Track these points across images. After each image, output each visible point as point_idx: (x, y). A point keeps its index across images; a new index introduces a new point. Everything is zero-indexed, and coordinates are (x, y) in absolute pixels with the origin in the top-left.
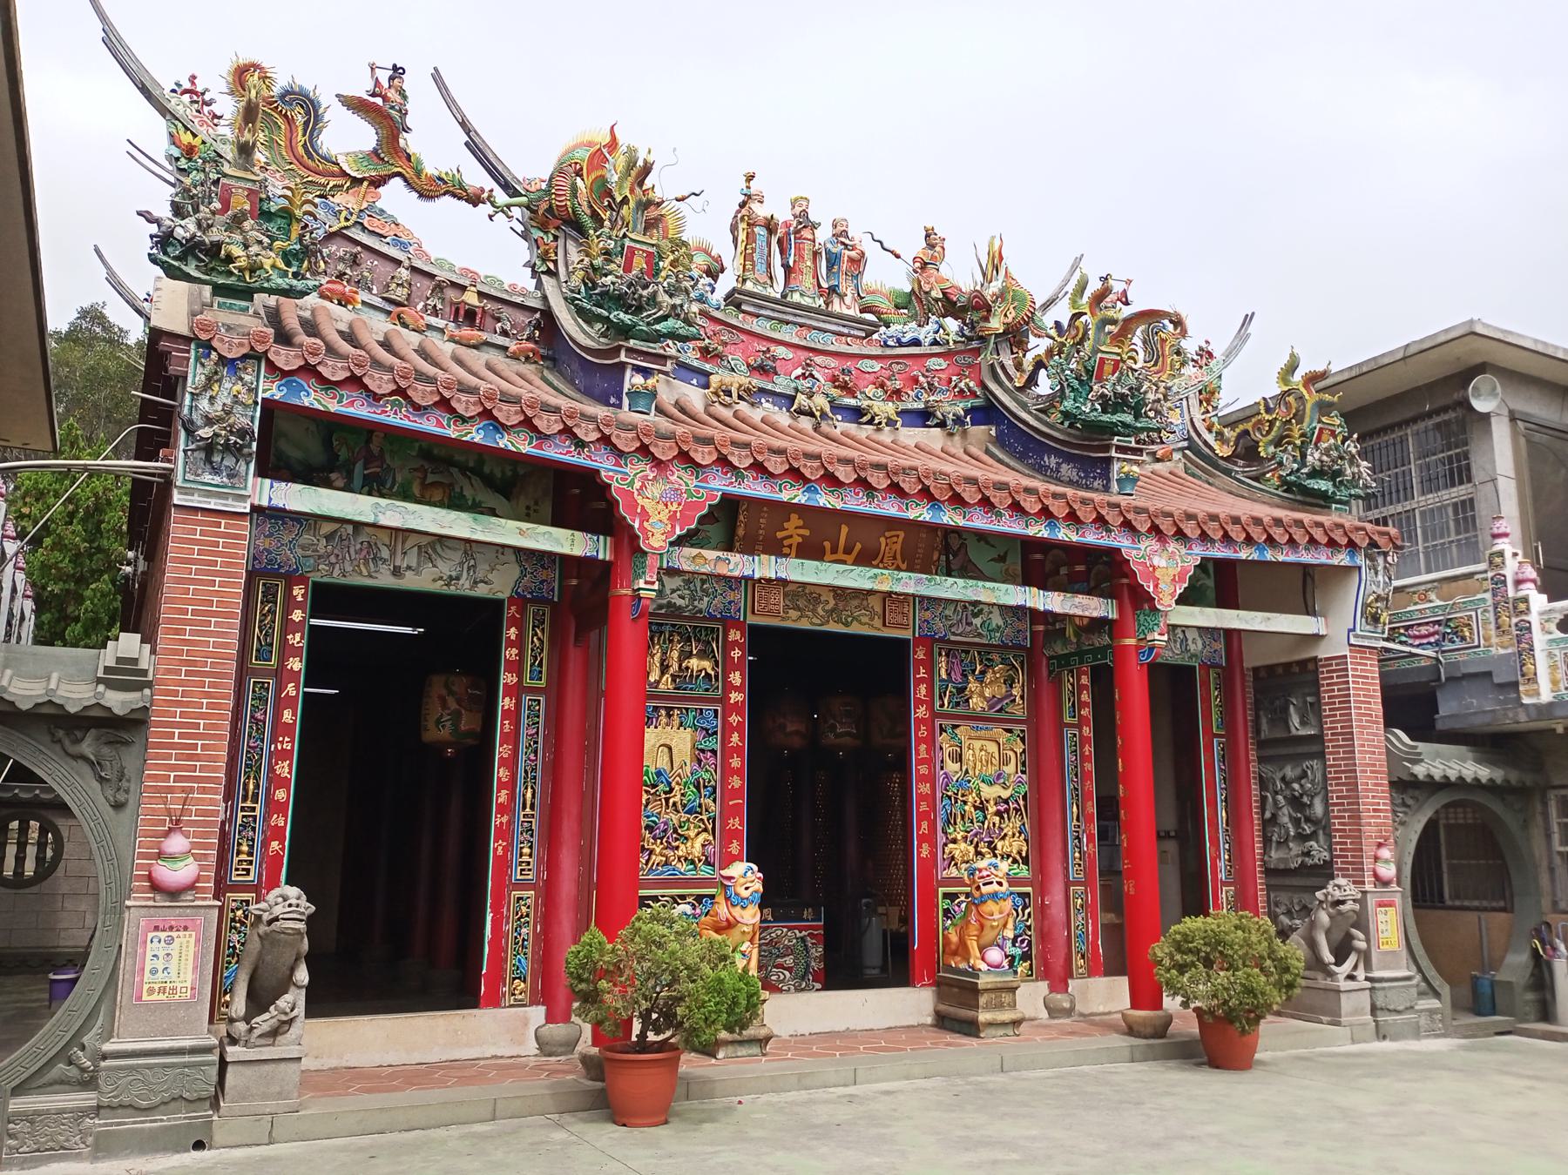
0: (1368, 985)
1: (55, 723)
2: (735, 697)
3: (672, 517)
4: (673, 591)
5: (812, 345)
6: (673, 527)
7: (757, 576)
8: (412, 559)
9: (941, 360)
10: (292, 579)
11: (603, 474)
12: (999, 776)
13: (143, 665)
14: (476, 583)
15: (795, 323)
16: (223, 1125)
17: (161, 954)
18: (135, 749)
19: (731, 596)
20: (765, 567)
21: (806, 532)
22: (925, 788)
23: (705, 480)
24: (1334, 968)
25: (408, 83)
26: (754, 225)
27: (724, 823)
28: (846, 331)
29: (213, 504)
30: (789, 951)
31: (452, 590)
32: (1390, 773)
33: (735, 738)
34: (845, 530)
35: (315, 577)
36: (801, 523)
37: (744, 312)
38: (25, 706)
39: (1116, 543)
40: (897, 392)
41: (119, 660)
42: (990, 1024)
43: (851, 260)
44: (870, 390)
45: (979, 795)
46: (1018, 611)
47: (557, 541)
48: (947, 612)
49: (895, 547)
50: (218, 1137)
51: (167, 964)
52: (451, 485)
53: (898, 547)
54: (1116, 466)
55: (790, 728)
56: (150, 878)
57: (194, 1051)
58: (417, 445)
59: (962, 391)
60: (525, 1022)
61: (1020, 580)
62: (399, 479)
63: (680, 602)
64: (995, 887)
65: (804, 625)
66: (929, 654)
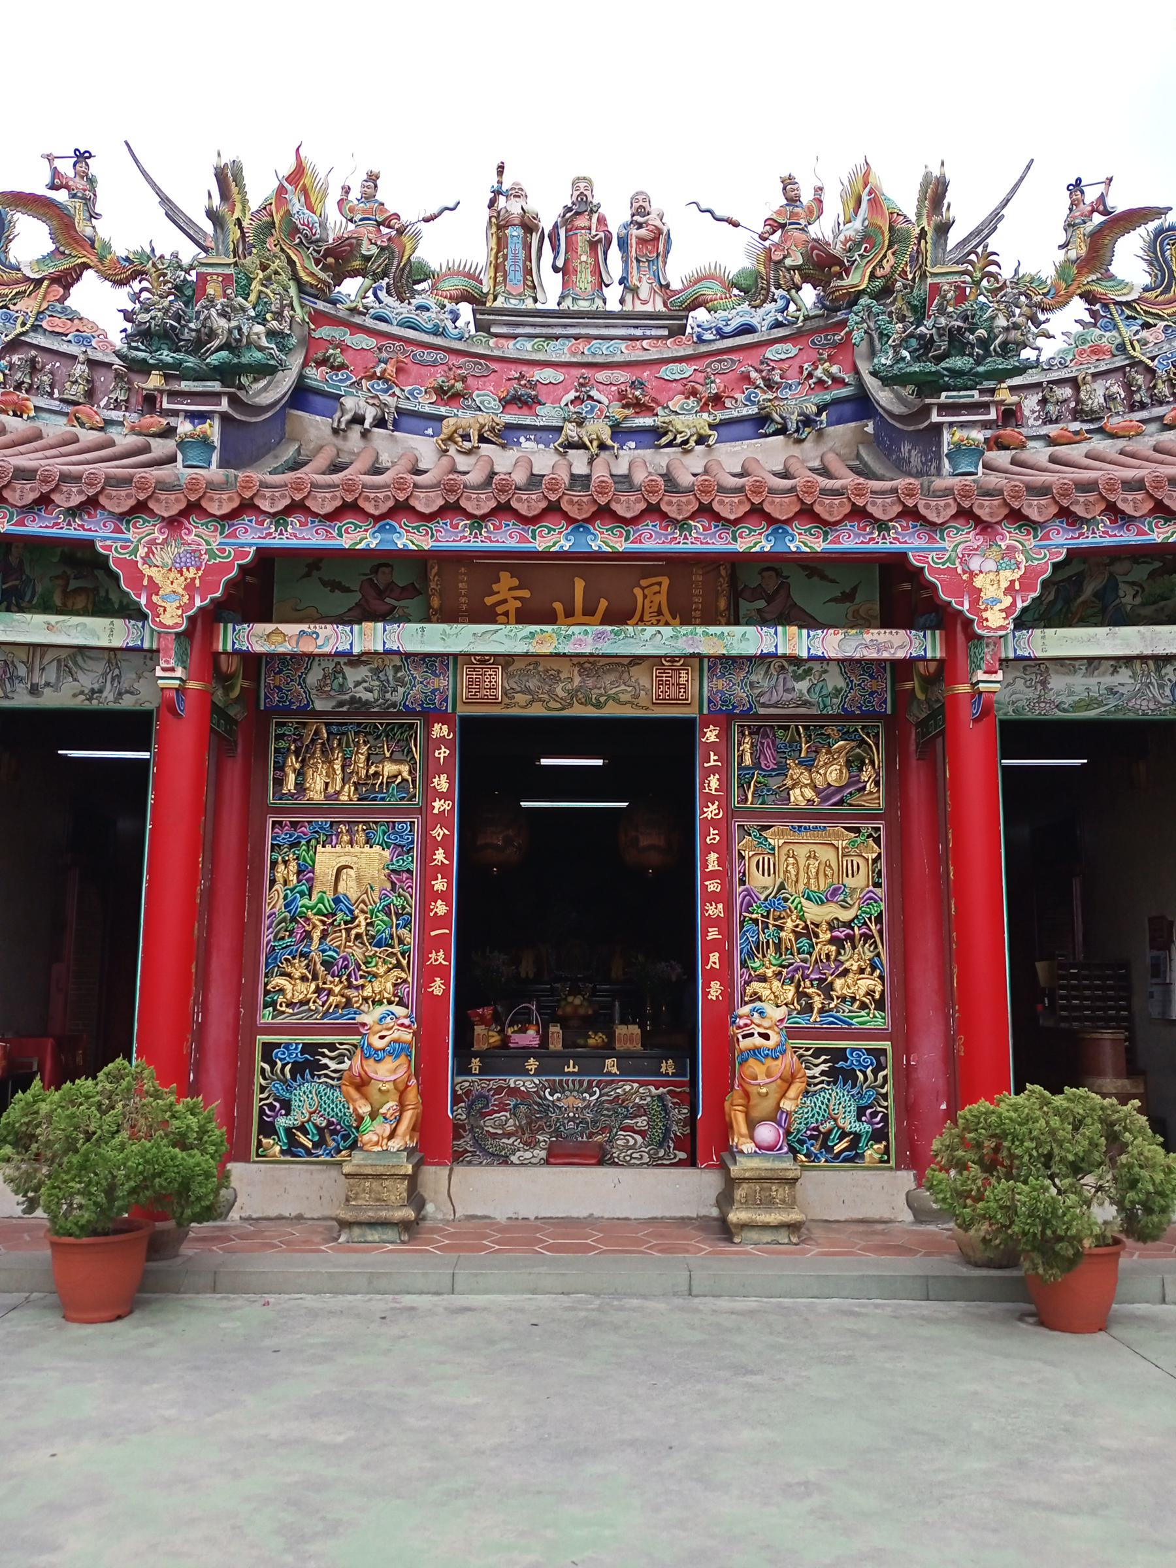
2: (438, 805)
3: (190, 587)
4: (357, 684)
5: (590, 360)
6: (192, 599)
7: (356, 651)
8: (51, 675)
9: (789, 346)
11: (98, 544)
12: (835, 892)
14: (120, 694)
15: (567, 337)
21: (526, 594)
22: (715, 910)
23: (233, 535)
25: (95, 167)
26: (506, 227)
27: (423, 957)
28: (639, 332)
30: (640, 1111)
31: (95, 704)
33: (440, 855)
34: (579, 585)
37: (496, 335)
40: (717, 400)
42: (744, 1226)
43: (642, 241)
44: (676, 403)
45: (802, 918)
46: (847, 664)
47: (93, 633)
48: (753, 678)
49: (657, 599)
52: (96, 590)
53: (663, 598)
54: (946, 437)
55: (644, 842)
58: (59, 550)
59: (820, 382)
62: (39, 589)
64: (757, 1041)
66: (725, 735)
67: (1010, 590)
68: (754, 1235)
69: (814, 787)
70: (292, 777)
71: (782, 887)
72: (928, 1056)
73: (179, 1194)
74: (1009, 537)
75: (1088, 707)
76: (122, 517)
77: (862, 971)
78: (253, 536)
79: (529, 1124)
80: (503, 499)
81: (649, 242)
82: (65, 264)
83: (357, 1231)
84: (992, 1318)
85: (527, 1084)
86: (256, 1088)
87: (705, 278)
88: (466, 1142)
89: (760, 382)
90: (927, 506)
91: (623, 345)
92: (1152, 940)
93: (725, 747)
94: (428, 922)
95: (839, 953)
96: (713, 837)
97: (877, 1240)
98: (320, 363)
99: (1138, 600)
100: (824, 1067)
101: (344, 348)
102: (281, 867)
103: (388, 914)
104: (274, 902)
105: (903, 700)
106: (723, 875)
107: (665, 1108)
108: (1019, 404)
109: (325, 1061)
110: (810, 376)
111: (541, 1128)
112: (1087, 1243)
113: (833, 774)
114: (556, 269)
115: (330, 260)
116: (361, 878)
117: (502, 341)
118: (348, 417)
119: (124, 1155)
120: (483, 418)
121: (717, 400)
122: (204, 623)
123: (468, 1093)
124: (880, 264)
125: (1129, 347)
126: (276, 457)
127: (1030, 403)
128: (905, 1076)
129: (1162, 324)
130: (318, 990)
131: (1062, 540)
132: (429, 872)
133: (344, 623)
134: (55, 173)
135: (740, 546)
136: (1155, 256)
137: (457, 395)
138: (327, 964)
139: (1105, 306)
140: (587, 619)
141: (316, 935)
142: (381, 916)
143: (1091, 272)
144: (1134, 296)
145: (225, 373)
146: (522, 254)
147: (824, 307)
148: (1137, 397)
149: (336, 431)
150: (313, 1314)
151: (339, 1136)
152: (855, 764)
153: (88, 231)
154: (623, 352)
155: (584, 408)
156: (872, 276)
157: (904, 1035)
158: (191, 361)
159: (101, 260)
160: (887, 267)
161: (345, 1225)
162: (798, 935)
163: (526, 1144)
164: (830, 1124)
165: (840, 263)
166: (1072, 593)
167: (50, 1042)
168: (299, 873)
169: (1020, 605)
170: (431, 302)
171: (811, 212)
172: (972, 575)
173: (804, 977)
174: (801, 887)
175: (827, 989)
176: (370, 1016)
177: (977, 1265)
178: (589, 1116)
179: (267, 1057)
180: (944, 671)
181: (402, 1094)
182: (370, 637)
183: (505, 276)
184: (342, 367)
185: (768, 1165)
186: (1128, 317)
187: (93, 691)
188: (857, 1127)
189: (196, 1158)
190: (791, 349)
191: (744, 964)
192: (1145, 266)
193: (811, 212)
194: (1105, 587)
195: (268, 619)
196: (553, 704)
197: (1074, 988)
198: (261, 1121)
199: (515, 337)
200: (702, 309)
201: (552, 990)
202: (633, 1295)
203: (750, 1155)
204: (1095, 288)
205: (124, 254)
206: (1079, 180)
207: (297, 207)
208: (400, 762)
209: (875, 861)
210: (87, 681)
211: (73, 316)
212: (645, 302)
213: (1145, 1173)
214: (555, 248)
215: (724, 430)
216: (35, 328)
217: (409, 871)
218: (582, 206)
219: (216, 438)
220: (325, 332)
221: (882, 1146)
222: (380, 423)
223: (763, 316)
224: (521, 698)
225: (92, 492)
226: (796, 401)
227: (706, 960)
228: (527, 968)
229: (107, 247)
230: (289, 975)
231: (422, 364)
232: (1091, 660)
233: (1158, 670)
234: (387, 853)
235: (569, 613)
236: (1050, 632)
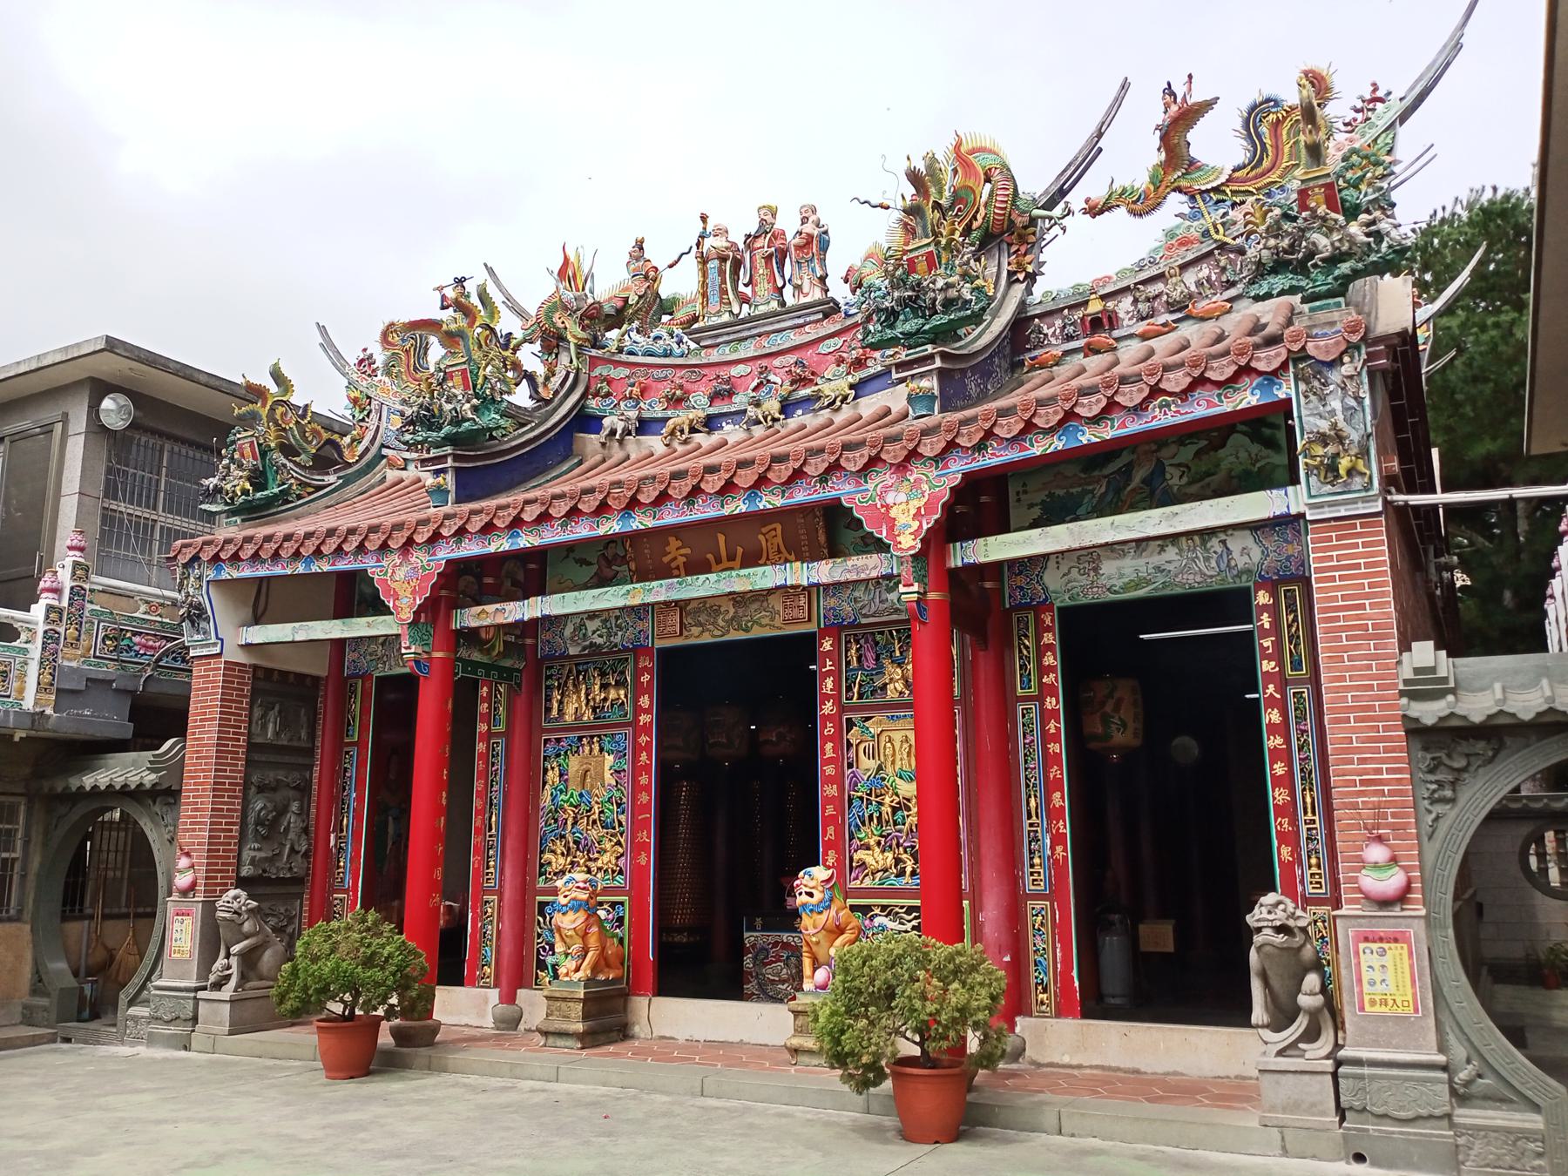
3: (414, 592)
10: (366, 677)
13: (1442, 673)
17: (1376, 966)
19: (640, 625)
20: (766, 577)
21: (687, 551)
34: (721, 538)
36: (679, 543)
38: (1527, 716)
39: (362, 566)
41: (1417, 671)
48: (856, 594)
53: (779, 540)
60: (486, 1001)
63: (599, 641)
65: (707, 639)
66: (837, 644)
67: (918, 515)
70: (555, 705)
71: (880, 768)
75: (1137, 586)
96: (829, 729)
99: (1185, 480)
100: (914, 923)
101: (609, 381)
102: (550, 773)
124: (975, 218)
125: (1212, 231)
129: (1251, 199)
134: (444, 298)
137: (679, 401)
140: (731, 564)
141: (570, 822)
143: (1175, 170)
144: (1223, 179)
154: (795, 338)
169: (925, 527)
172: (888, 507)
173: (898, 845)
181: (584, 936)
184: (608, 395)
186: (1218, 201)
194: (1152, 473)
199: (717, 345)
204: (1183, 183)
232: (1139, 541)
233: (1204, 543)
235: (719, 561)
236: (991, 539)
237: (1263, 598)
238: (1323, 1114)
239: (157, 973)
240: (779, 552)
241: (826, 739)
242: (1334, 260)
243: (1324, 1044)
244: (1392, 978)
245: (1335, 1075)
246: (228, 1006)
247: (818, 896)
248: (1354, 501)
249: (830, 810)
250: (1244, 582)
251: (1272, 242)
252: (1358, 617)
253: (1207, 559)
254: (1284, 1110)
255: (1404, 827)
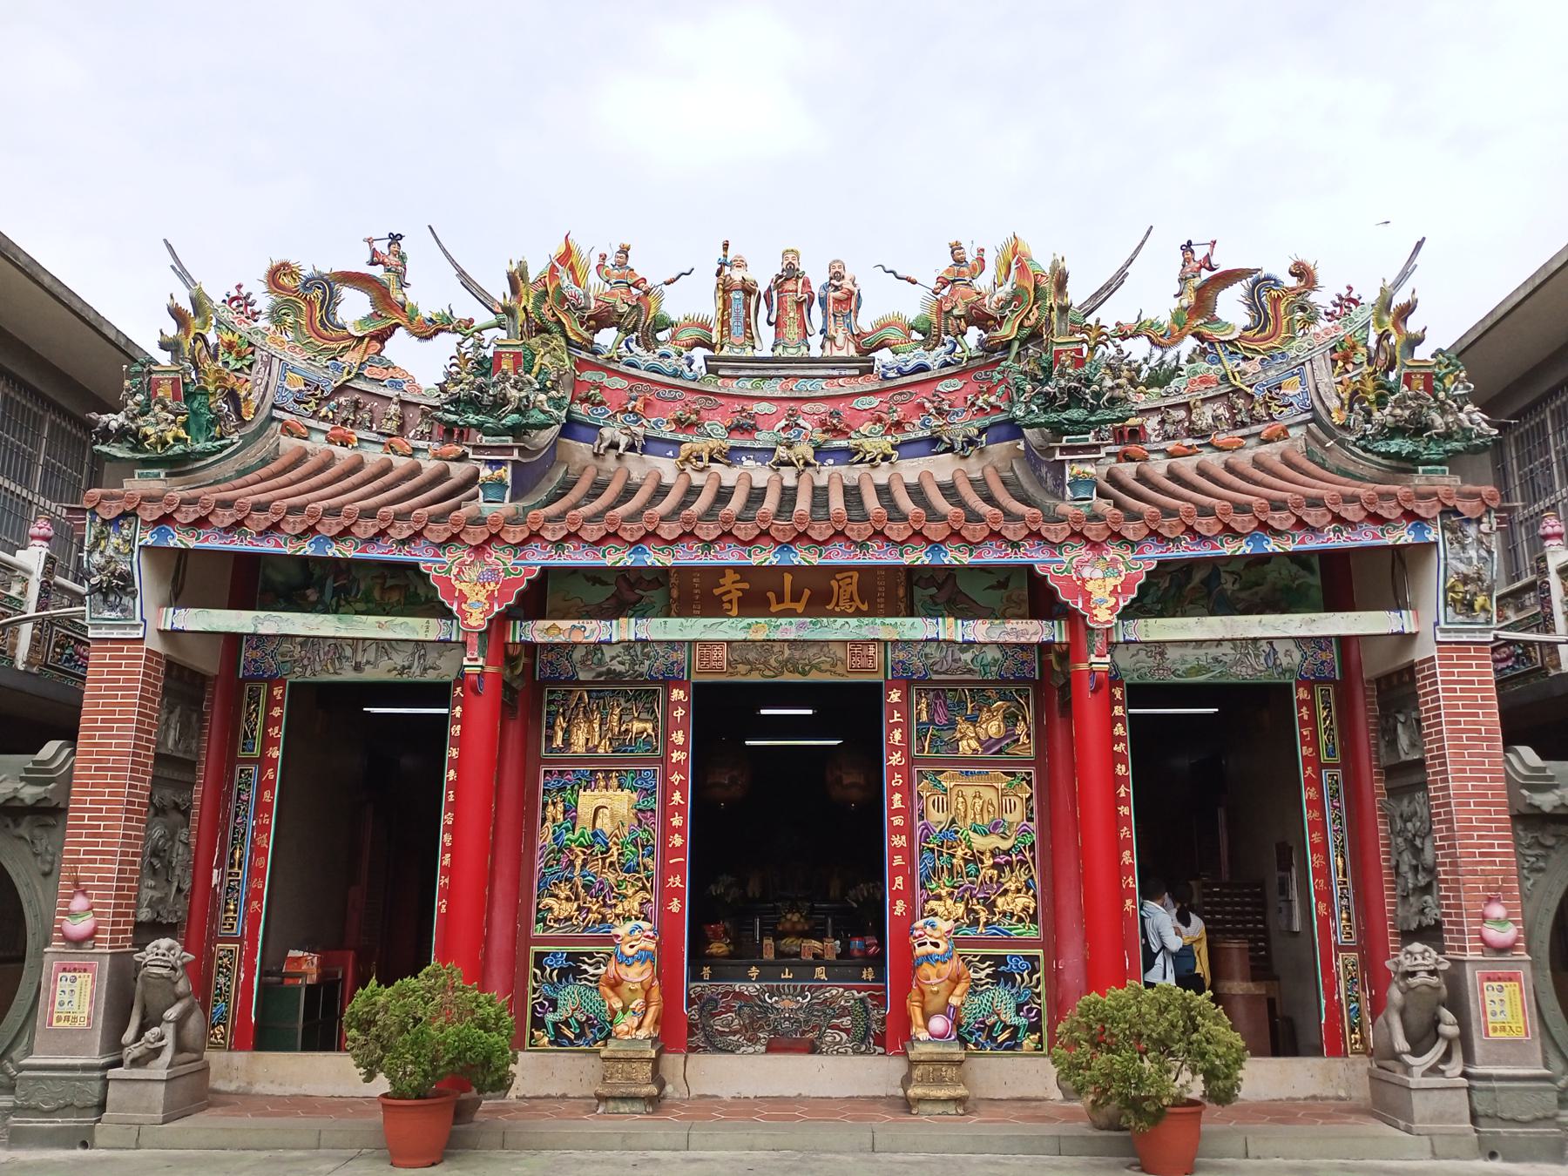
0: (1464, 1082)
1: (8, 813)
2: (677, 756)
3: (490, 597)
4: (613, 658)
6: (492, 606)
9: (955, 381)
10: (273, 681)
12: (996, 826)
14: (425, 669)
16: (104, 1130)
17: (67, 990)
18: (59, 829)
22: (900, 841)
24: (1409, 1059)
27: (664, 881)
28: (836, 373)
29: (116, 634)
30: (845, 1012)
32: (1511, 806)
33: (677, 797)
35: (292, 679)
40: (898, 425)
42: (920, 1100)
43: (838, 301)
45: (969, 847)
47: (414, 630)
48: (927, 650)
49: (849, 589)
50: (98, 1140)
51: (72, 998)
52: (407, 587)
53: (854, 588)
55: (847, 780)
56: (1482, 939)
57: (85, 1068)
59: (981, 409)
61: (1025, 608)
62: (362, 587)
64: (929, 948)
66: (906, 697)
67: (1114, 592)
68: (928, 1108)
69: (978, 739)
70: (560, 734)
71: (953, 821)
72: (1072, 961)
73: (483, 1066)
74: (1112, 552)
76: (439, 545)
77: (1019, 891)
78: (538, 558)
79: (751, 1023)
80: (727, 528)
81: (846, 302)
82: (381, 325)
83: (611, 1104)
84: (1108, 1167)
85: (750, 988)
86: (530, 989)
87: (889, 325)
88: (698, 1039)
89: (932, 411)
90: (1048, 530)
91: (823, 383)
92: (1279, 862)
93: (905, 705)
94: (667, 851)
95: (1000, 876)
97: (1029, 1112)
98: (583, 401)
99: (1237, 586)
100: (988, 971)
101: (601, 388)
102: (551, 808)
103: (636, 846)
104: (546, 836)
105: (1045, 666)
106: (906, 812)
107: (866, 1010)
108: (1142, 426)
109: (585, 967)
110: (973, 404)
111: (761, 1027)
112: (1165, 1101)
113: (994, 728)
114: (770, 324)
115: (592, 323)
116: (615, 813)
117: (728, 381)
118: (605, 444)
119: (445, 1032)
120: (713, 443)
121: (898, 425)
122: (500, 622)
123: (700, 997)
124: (1027, 317)
126: (550, 480)
127: (1152, 423)
128: (1054, 977)
129: (1259, 357)
130: (579, 909)
131: (1153, 554)
132: (667, 811)
133: (606, 619)
134: (374, 253)
135: (906, 560)
136: (1253, 301)
137: (692, 425)
138: (586, 887)
139: (1212, 344)
140: (793, 605)
141: (579, 862)
142: (630, 847)
143: (1199, 317)
144: (1236, 335)
145: (517, 431)
146: (743, 313)
147: (984, 350)
148: (1238, 418)
149: (596, 455)
150: (582, 1163)
151: (593, 1030)
152: (1011, 719)
153: (400, 298)
155: (792, 434)
156: (1021, 326)
157: (1052, 943)
158: (491, 422)
159: (411, 321)
160: (1033, 318)
161: (602, 1099)
162: (967, 861)
163: (749, 1040)
164: (993, 1019)
165: (995, 319)
166: (1169, 590)
167: (351, 955)
168: (565, 812)
169: (1122, 604)
170: (671, 352)
171: (974, 269)
172: (1084, 581)
174: (969, 821)
175: (991, 906)
176: (622, 929)
177: (1101, 1129)
178: (802, 1016)
179: (539, 963)
180: (1068, 654)
181: (647, 993)
182: (626, 629)
183: (729, 330)
184: (601, 403)
185: (940, 1050)
187: (404, 668)
188: (1016, 1021)
189: (495, 1038)
190: (957, 383)
191: (923, 886)
192: (1245, 309)
193: (974, 269)
195: (543, 618)
196: (767, 673)
197: (1217, 904)
198: (533, 1016)
199: (738, 377)
200: (886, 350)
201: (775, 908)
202: (830, 1152)
203: (925, 1042)
204: (1204, 330)
205: (428, 316)
206: (1190, 243)
207: (567, 283)
208: (646, 721)
209: (1028, 800)
210: (399, 659)
211: (389, 366)
212: (840, 349)
213: (1210, 1047)
214: (769, 306)
215: (904, 449)
216: (358, 376)
217: (652, 810)
218: (791, 273)
219: (508, 480)
220: (588, 376)
221: (1036, 1037)
222: (631, 448)
223: (935, 357)
224: (742, 668)
225: (418, 527)
226: (962, 426)
227: (892, 883)
228: (754, 889)
229: (415, 310)
230: (556, 896)
231: (664, 400)
234: (635, 796)
237: (1303, 694)
238: (1461, 1121)
239: (22, 1047)
240: (852, 599)
241: (894, 790)
242: (1448, 436)
243: (1455, 1067)
244: (1505, 1008)
245: (1470, 1089)
246: (162, 1087)
247: (943, 946)
248: (1473, 631)
249: (898, 860)
250: (1286, 679)
251: (1398, 411)
252: (1475, 723)
253: (1257, 656)
254: (1432, 1121)
255: (1511, 889)
